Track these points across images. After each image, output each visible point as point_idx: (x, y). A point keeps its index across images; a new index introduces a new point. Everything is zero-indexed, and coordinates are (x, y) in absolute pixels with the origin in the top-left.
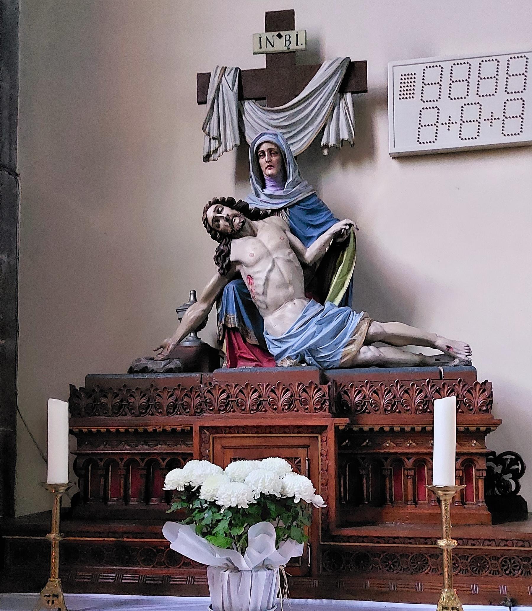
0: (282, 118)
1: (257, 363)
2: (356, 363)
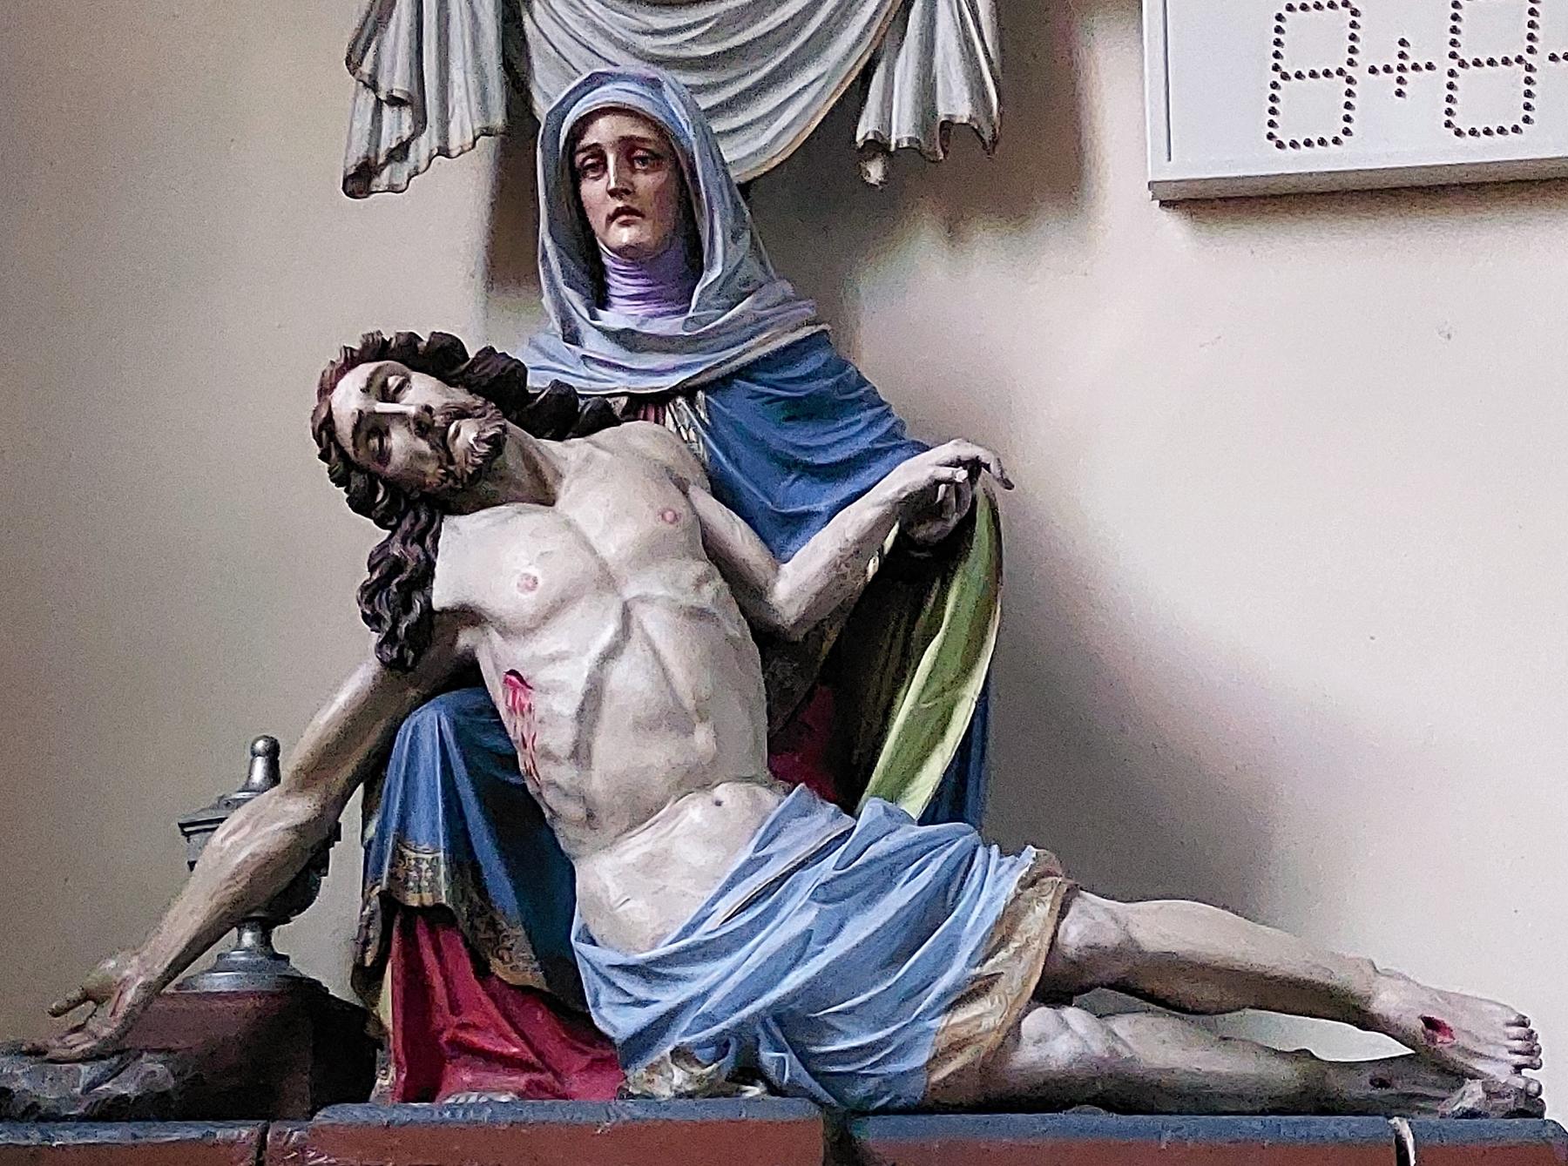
0: (689, 27)
1: (536, 1077)
2: (993, 1090)
